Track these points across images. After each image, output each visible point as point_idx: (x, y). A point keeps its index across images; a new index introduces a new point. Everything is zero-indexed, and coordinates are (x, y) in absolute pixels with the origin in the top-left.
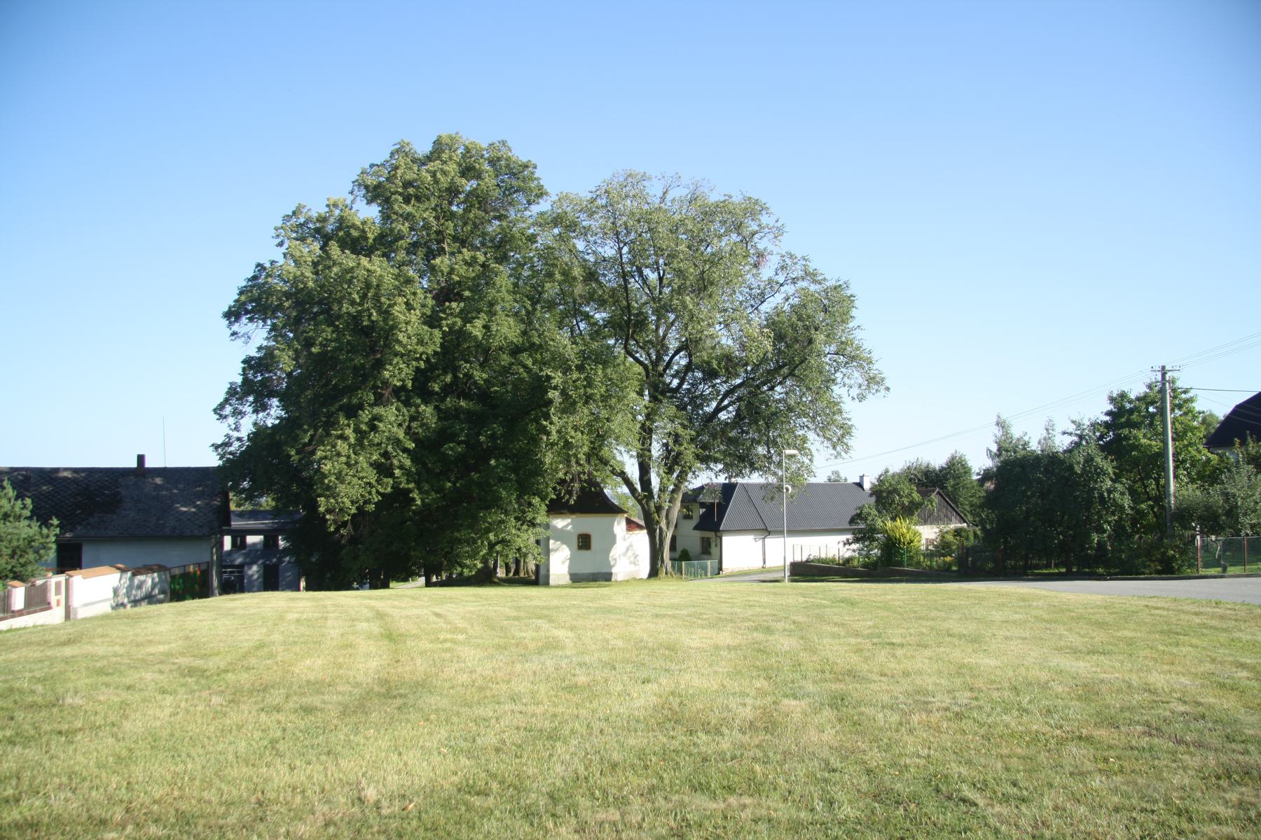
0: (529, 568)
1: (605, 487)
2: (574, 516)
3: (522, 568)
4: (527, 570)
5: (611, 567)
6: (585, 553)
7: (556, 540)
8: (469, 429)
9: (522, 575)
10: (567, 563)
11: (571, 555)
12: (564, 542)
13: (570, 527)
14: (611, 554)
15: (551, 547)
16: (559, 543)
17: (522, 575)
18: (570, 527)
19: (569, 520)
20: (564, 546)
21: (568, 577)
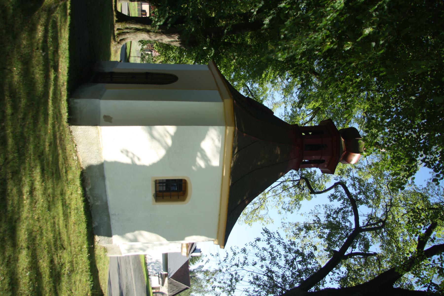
0: (127, 36)
1: (239, 89)
2: (226, 173)
3: (127, 26)
4: (124, 33)
5: (122, 234)
6: (150, 191)
7: (174, 138)
8: (353, 45)
9: (118, 26)
10: (126, 160)
11: (144, 167)
12: (170, 151)
13: (202, 164)
14: (146, 234)
15: (159, 129)
16: (169, 142)
17: (118, 26)
18: (202, 164)
19: (216, 162)
20: (162, 153)
21: (94, 162)
